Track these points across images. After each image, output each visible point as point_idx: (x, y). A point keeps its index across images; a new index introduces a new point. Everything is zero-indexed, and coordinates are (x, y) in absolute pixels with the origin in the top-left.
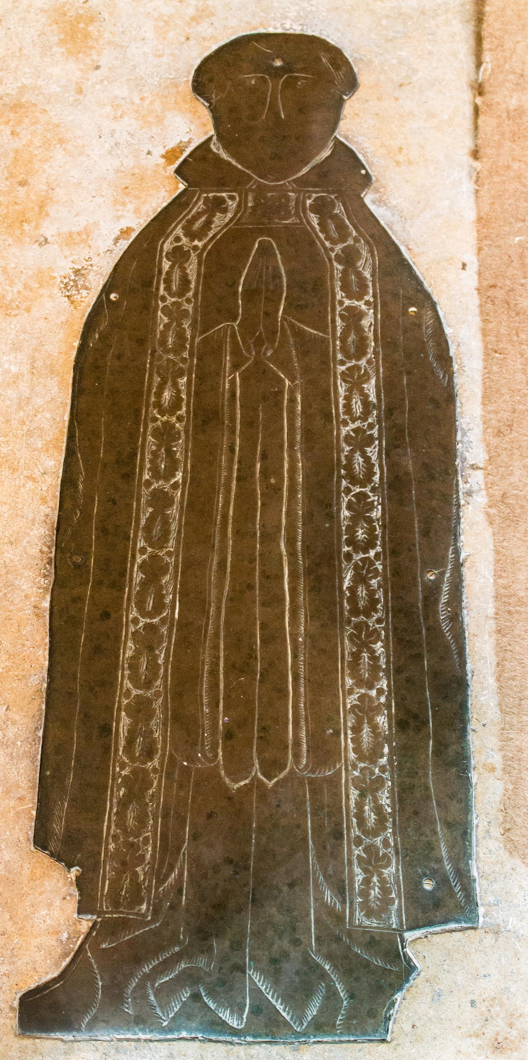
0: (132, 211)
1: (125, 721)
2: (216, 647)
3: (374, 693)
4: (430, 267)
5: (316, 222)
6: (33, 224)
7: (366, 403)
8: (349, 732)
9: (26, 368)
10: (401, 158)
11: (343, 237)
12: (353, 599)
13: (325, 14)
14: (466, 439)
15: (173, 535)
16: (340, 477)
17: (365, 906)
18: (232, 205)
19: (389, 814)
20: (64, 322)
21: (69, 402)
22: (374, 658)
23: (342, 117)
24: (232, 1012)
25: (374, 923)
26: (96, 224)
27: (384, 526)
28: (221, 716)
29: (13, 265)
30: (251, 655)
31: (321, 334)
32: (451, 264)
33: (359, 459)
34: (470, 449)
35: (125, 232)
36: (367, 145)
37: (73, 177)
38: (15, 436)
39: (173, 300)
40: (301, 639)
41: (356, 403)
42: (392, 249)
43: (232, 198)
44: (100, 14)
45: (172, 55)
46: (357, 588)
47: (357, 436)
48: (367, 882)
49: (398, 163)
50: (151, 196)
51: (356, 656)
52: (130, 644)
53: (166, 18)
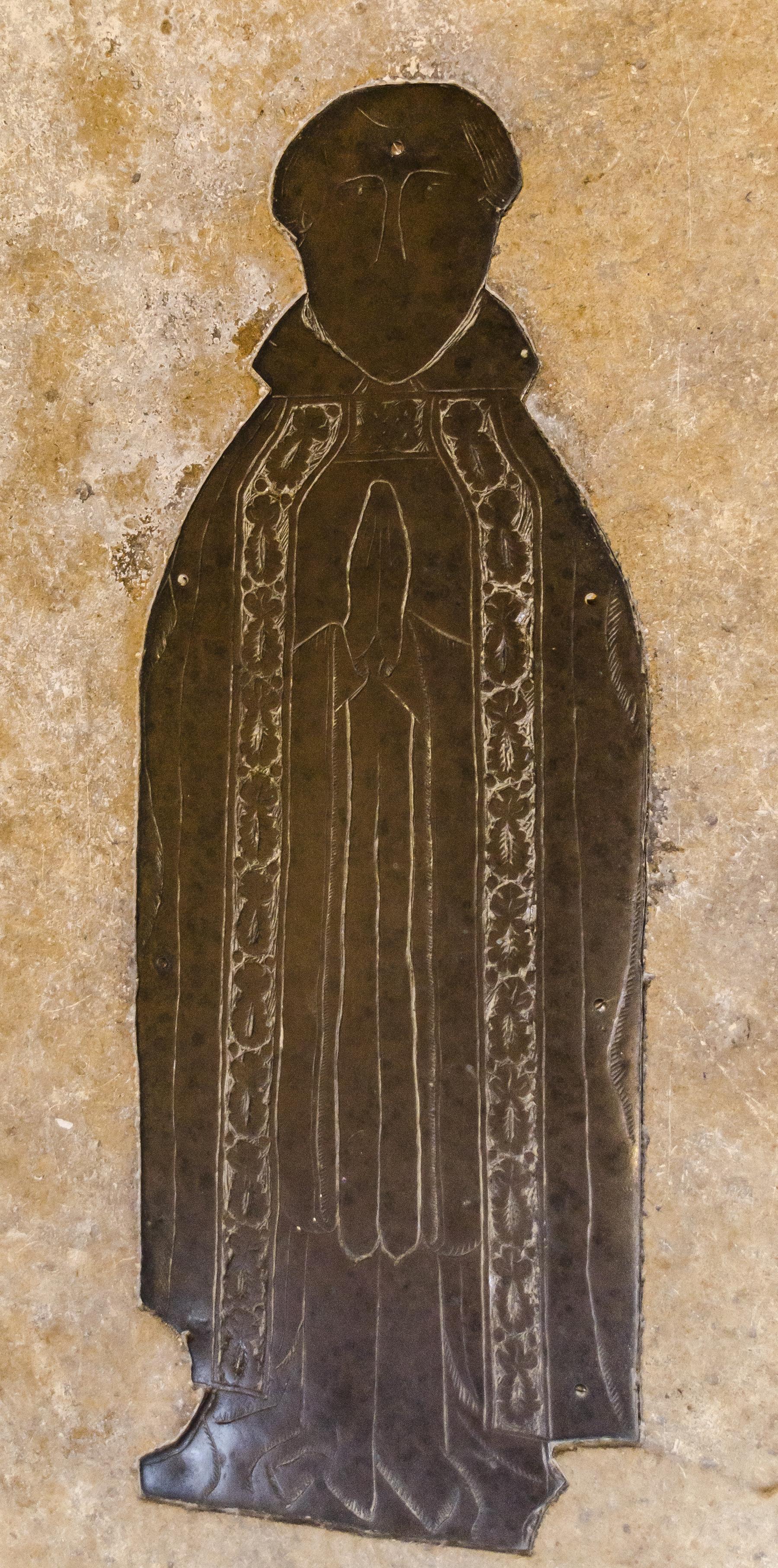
0: (197, 437)
1: (227, 1173)
2: (329, 1089)
3: (521, 1158)
4: (620, 523)
5: (453, 450)
6: (71, 464)
7: (519, 751)
8: (490, 1204)
9: (80, 691)
10: (582, 325)
11: (494, 470)
12: (497, 1034)
13: (470, 39)
14: (658, 803)
15: (272, 937)
16: (482, 862)
17: (506, 1407)
18: (334, 422)
19: (537, 1306)
20: (122, 620)
21: (137, 740)
22: (522, 1114)
23: (494, 250)
24: (359, 1504)
25: (515, 1428)
26: (152, 459)
27: (538, 936)
28: (337, 1175)
29: (51, 532)
30: (372, 1103)
31: (459, 640)
32: (650, 517)
33: (507, 834)
34: (663, 820)
35: (191, 473)
36: (530, 303)
37: (117, 380)
38: (77, 789)
39: (259, 584)
40: (431, 1084)
41: (506, 750)
42: (563, 490)
43: (333, 412)
44: (132, 74)
45: (241, 144)
46: (502, 1019)
47: (506, 802)
48: (508, 1382)
49: (577, 335)
50: (222, 410)
51: (500, 1111)
52: (228, 1077)
53: (227, 74)
